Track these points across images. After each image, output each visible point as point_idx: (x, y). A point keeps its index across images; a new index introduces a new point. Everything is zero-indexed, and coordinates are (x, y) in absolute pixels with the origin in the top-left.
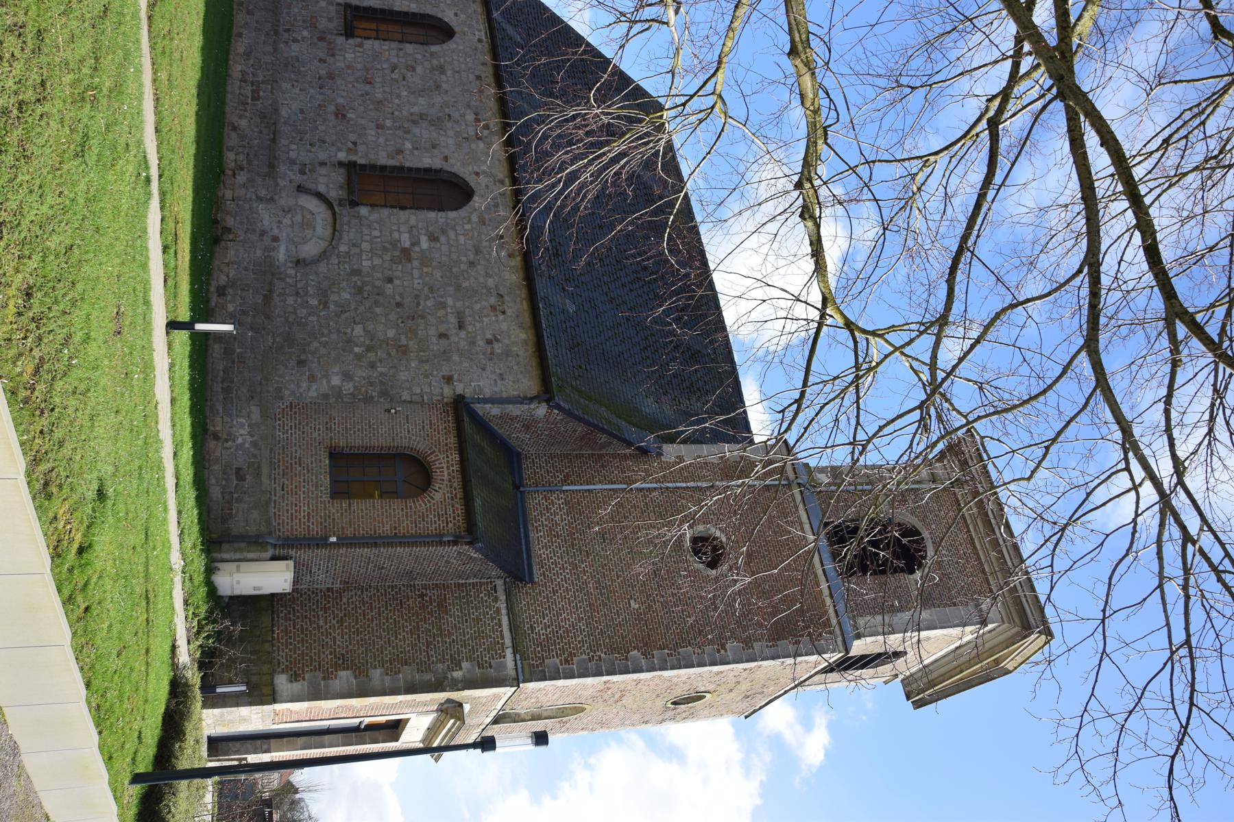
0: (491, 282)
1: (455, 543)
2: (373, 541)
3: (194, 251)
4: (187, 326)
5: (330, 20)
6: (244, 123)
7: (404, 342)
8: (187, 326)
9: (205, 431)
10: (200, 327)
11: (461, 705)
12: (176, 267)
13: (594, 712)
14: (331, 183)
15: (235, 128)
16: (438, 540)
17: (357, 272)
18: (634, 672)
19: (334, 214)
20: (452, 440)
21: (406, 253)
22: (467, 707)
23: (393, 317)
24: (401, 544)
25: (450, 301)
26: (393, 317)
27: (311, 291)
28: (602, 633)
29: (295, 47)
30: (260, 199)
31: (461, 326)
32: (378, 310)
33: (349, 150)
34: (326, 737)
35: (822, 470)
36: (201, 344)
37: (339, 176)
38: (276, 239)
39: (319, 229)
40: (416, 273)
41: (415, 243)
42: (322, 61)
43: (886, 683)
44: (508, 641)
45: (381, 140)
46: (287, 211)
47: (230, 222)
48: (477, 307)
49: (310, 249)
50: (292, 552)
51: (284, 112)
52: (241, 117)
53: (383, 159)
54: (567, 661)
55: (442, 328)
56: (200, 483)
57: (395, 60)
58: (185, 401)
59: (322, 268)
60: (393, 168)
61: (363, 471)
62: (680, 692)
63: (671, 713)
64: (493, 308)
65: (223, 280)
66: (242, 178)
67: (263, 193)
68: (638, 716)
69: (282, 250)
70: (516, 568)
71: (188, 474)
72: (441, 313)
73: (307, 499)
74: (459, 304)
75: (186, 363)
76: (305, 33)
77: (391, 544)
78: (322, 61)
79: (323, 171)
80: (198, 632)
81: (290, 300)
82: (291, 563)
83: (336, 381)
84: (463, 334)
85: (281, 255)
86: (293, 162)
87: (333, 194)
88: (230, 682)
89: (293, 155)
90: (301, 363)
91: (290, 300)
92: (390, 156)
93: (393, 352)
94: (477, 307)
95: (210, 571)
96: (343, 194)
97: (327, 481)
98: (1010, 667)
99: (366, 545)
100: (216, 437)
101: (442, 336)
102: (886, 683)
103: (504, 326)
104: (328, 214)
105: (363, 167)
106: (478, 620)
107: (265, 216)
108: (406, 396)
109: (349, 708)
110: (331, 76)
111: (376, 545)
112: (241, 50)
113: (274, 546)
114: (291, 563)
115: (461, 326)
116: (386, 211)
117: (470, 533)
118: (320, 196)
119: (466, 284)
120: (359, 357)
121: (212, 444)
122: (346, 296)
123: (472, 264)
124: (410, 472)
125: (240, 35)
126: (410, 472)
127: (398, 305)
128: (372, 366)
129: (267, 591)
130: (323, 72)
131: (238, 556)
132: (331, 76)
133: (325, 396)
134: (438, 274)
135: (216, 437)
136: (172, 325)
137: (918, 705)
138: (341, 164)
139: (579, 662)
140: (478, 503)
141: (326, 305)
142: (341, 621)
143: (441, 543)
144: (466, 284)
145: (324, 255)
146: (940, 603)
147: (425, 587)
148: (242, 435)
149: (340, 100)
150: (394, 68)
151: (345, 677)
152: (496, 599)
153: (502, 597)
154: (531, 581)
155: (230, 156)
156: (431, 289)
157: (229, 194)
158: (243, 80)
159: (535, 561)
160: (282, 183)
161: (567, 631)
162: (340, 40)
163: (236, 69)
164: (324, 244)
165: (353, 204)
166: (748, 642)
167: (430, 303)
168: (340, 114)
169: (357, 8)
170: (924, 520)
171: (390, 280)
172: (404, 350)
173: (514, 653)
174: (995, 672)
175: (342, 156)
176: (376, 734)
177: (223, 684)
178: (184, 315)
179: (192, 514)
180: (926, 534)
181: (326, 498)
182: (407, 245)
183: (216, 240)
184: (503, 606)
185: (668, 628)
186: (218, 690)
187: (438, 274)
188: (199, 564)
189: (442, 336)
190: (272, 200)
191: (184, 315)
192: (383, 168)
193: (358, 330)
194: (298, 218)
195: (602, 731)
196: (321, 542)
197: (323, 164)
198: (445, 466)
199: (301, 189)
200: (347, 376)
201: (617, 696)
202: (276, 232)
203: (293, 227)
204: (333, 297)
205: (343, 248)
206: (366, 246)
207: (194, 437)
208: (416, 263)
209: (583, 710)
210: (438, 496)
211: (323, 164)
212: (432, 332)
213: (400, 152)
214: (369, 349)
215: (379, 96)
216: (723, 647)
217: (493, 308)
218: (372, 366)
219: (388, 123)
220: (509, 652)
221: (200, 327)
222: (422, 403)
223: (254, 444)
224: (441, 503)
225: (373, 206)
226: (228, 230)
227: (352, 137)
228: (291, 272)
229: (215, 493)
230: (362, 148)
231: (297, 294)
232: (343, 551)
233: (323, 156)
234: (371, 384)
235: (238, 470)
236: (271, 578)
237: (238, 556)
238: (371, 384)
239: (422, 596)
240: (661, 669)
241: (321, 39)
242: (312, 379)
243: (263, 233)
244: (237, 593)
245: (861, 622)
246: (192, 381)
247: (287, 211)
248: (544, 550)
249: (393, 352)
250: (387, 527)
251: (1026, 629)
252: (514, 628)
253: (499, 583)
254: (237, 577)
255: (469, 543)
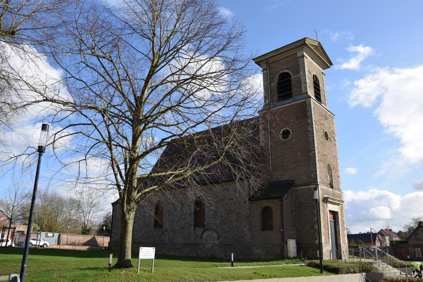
0: (221, 192)
1: (282, 201)
2: (282, 221)
3: (217, 262)
4: (232, 262)
5: (158, 231)
6: (186, 252)
7: (236, 213)
8: (232, 262)
9: (258, 259)
10: (232, 260)
11: (324, 198)
12: (148, 112)
13: (330, 160)
14: (199, 231)
15: (187, 254)
16: (282, 205)
17: (220, 224)
18: (315, 154)
19: (207, 230)
20: (259, 202)
21: (215, 212)
22: (325, 196)
23: (231, 216)
24: (283, 214)
25: (226, 202)
26: (231, 216)
27: (225, 235)
28: (306, 163)
29: (166, 240)
30: (204, 247)
31: (232, 199)
32: (229, 219)
33: (191, 226)
34: (337, 230)
35: (265, 102)
36: (236, 260)
37: (198, 229)
38: (213, 244)
39: (210, 233)
40: (220, 210)
41: (213, 210)
42: (169, 233)
43: (325, 75)
44: (308, 187)
45: (188, 218)
46: (206, 241)
47: (210, 254)
48: (227, 195)
49: (215, 235)
50: (285, 239)
51: (183, 242)
52: (184, 252)
53: (193, 218)
54: (313, 172)
55: (233, 204)
56: (268, 260)
57: (168, 215)
58: (249, 263)
59: (220, 232)
60: (195, 215)
61: (266, 224)
62: (323, 139)
63: (332, 139)
64: (227, 191)
65: (223, 256)
66: (199, 252)
67: (202, 247)
68: (332, 148)
69: (216, 242)
70: (290, 184)
71: (266, 263)
72: (229, 204)
73: (273, 236)
74: (227, 199)
75: (241, 263)
76: (162, 237)
77: (283, 216)
78: (169, 233)
79: (196, 232)
80: (303, 261)
81: (228, 240)
82: (288, 240)
83: (246, 229)
84: (234, 199)
85: (217, 242)
86: (194, 240)
87: (202, 230)
88: (317, 254)
89: (193, 240)
90: (242, 238)
91: (228, 240)
92: (192, 216)
93: (239, 215)
94: (227, 195)
95: (289, 258)
96: (202, 228)
97: (269, 231)
98: (317, 43)
99: (283, 222)
100: (259, 257)
101: (235, 204)
102: (325, 75)
103: (232, 188)
104: (207, 231)
105: (195, 223)
106: (303, 194)
107: (208, 246)
108: (249, 213)
109: (324, 225)
110: (173, 231)
111: (283, 220)
112: (168, 252)
113: (284, 244)
114: (288, 240)
115: (232, 199)
116: (206, 217)
117: (280, 198)
118: (203, 233)
119: (222, 198)
120: (240, 224)
121: (261, 258)
122: (226, 227)
123: (217, 196)
124: (266, 213)
125: (164, 253)
126: (266, 213)
127: (228, 214)
128: (242, 220)
129: (295, 245)
130: (172, 233)
131: (286, 252)
132: (173, 231)
133: (250, 232)
134: (220, 204)
135: (259, 257)
136: (232, 266)
137: (331, 64)
138: (194, 228)
139: (313, 169)
140: (273, 196)
141: (229, 232)
142: (303, 227)
143: (282, 205)
144: (222, 198)
145: (217, 232)
146: (299, 67)
147: (295, 207)
148: (259, 251)
149: (179, 228)
150: (170, 215)
151: (316, 227)
152: (298, 189)
153: (297, 188)
154: (294, 180)
155: (194, 255)
156: (224, 206)
157: (203, 255)
158: (175, 252)
159: (289, 179)
160: (200, 242)
161: (306, 171)
162: (163, 228)
163: (173, 253)
164: (214, 232)
165: (204, 225)
166: (308, 124)
167: (227, 207)
168: (182, 228)
169: (155, 224)
170: (277, 73)
171: (222, 216)
172: (238, 213)
173: (311, 185)
174: (320, 47)
175: (192, 228)
176: (336, 217)
177: (317, 256)
178: (230, 263)
179: (275, 262)
180: (281, 72)
181: (273, 232)
182: (213, 212)
183: (214, 258)
184: (299, 188)
185: (304, 146)
186: (232, 254)
187: (220, 204)
188: (287, 261)
189: (235, 204)
190: (204, 245)
191: (230, 263)
192: (195, 218)
193: (234, 224)
194: (208, 238)
195: (337, 156)
196: (283, 233)
197: (195, 233)
198: (265, 203)
199: (201, 238)
200: (245, 227)
201: (324, 156)
202: (212, 244)
203: (210, 239)
204: (227, 230)
205: (215, 228)
206: (214, 222)
207: (258, 262)
208: (218, 210)
209: (329, 165)
210: (272, 205)
211: (195, 233)
212: (234, 206)
213: (191, 214)
214: (238, 221)
215: (177, 219)
216: (309, 131)
217: (227, 191)
218: (242, 220)
219: (184, 216)
220: (310, 186)
221: (232, 260)
222: (251, 209)
223: (261, 248)
224: (273, 204)
225: (204, 220)
226: (212, 255)
227: (188, 225)
228: (221, 240)
229: (272, 257)
230: (190, 223)
231: (226, 238)
232: (285, 228)
233: (193, 233)
234: (246, 221)
235: (267, 252)
236: (292, 244)
237: (286, 252)
238: (246, 221)
239: (297, 208)
240: (314, 148)
241: (164, 233)
242: (246, 235)
243: (212, 247)
244: (296, 252)
245: (303, 92)
246: (245, 262)
247: (206, 241)
248: (286, 177)
249: (239, 215)
250: (279, 217)
251: (305, 44)
252: (305, 185)
253: (294, 189)
254: (291, 252)
255: (282, 198)
